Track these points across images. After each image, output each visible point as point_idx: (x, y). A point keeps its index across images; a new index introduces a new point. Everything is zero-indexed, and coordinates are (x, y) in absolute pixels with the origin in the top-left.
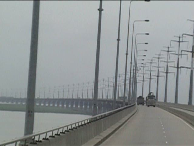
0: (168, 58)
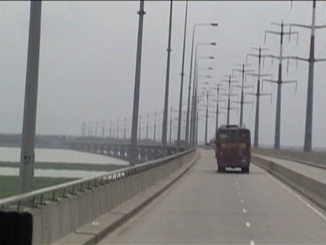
0: (243, 81)
